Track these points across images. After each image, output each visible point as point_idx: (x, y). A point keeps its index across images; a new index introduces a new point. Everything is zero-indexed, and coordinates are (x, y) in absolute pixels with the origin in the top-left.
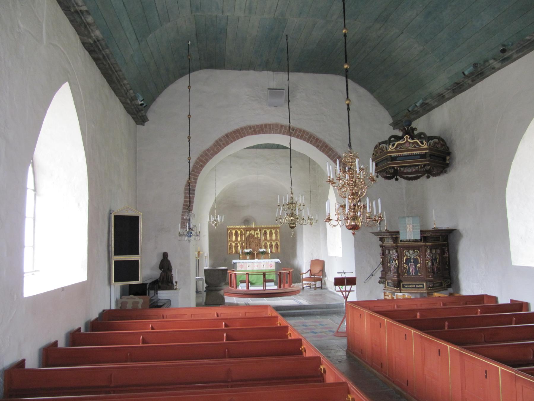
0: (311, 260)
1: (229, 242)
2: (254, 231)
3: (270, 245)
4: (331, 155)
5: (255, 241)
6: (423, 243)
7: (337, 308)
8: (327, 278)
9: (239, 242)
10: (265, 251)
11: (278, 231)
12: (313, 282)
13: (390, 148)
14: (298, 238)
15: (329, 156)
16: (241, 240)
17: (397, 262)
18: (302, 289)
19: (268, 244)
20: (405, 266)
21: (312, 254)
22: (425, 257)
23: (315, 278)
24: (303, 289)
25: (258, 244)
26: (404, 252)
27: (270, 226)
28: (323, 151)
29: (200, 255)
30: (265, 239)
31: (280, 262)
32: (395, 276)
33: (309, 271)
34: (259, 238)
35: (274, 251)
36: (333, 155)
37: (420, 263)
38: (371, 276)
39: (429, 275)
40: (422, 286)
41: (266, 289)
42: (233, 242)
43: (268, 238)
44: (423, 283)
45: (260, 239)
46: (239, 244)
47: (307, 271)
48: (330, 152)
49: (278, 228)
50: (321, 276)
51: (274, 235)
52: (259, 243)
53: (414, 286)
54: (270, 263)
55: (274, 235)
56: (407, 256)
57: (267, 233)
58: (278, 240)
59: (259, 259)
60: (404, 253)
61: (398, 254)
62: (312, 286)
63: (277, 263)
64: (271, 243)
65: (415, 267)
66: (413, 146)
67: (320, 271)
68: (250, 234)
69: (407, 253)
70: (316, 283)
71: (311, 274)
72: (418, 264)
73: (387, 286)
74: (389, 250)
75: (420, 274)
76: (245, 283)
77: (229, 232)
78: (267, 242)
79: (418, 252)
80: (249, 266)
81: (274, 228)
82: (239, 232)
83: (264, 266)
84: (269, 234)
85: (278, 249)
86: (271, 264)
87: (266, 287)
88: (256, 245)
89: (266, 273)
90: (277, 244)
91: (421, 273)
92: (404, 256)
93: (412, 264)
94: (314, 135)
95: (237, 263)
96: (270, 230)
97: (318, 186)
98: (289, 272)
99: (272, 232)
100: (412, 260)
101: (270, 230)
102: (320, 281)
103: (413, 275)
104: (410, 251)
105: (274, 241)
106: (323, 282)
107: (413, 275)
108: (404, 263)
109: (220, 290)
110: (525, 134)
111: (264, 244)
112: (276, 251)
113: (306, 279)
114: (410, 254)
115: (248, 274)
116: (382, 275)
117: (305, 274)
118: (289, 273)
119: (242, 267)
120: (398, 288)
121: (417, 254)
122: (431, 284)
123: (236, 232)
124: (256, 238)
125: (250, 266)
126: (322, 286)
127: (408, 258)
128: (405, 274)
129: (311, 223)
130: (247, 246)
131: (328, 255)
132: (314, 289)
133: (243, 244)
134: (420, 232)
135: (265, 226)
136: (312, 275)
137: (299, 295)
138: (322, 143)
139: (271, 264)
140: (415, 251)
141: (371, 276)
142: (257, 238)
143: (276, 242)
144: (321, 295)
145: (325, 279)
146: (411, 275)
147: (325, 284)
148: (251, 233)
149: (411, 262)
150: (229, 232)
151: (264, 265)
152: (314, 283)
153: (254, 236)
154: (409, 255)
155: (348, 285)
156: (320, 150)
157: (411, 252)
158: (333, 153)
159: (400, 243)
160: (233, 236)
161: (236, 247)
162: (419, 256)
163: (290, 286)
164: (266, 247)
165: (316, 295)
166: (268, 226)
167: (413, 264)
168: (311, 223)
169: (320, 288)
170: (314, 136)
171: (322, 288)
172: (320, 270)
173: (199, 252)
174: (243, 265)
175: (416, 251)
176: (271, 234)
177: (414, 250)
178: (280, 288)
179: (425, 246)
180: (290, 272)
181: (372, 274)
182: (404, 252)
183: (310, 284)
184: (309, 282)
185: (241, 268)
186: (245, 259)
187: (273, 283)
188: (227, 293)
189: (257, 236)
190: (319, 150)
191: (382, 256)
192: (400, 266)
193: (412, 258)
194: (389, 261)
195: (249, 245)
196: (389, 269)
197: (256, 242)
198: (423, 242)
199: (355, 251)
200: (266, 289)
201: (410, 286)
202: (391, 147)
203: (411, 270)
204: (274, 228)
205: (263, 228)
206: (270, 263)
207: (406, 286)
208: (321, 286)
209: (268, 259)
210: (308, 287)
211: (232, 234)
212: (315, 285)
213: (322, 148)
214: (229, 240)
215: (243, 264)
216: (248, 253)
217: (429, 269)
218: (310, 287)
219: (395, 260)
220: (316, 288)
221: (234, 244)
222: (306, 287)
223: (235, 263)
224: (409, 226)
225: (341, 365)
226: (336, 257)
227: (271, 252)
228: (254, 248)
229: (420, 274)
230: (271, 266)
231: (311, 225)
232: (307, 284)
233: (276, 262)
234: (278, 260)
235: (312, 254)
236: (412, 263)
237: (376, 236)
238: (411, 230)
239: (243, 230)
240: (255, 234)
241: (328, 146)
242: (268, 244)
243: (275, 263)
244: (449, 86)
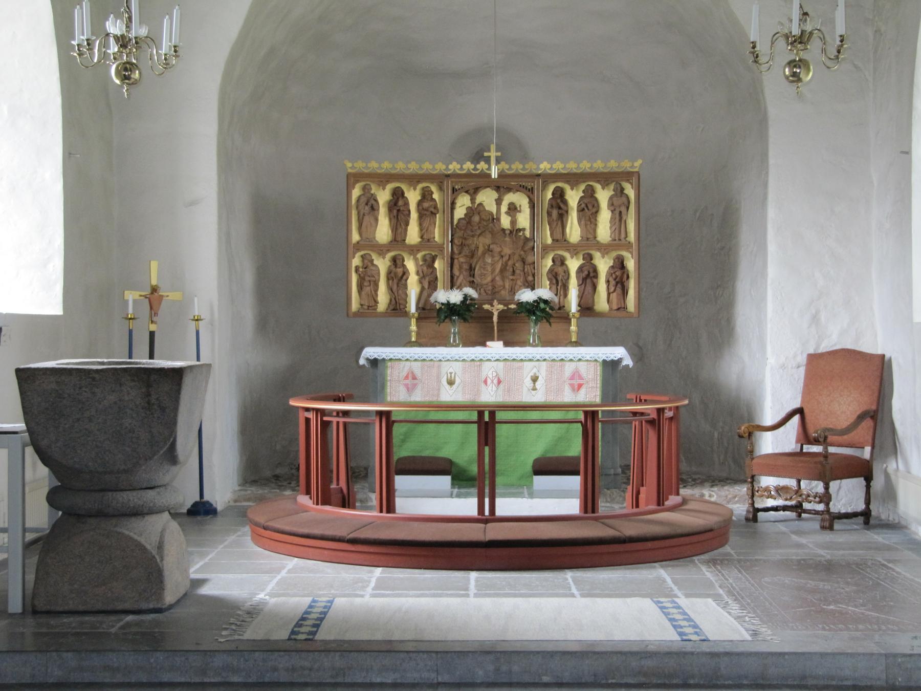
0: (812, 351)
1: (358, 250)
2: (494, 195)
3: (580, 270)
5: (496, 249)
9: (413, 250)
10: (546, 302)
11: (630, 192)
12: (815, 483)
14: (746, 236)
16: (426, 239)
18: (747, 519)
19: (574, 264)
21: (815, 319)
23: (826, 455)
24: (755, 519)
25: (519, 265)
27: (585, 166)
29: (163, 309)
30: (558, 236)
31: (628, 361)
33: (796, 419)
34: (524, 230)
35: (602, 302)
41: (499, 512)
42: (381, 250)
43: (574, 231)
45: (527, 240)
46: (410, 265)
47: (782, 415)
49: (628, 175)
50: (868, 449)
51: (605, 216)
52: (524, 261)
54: (569, 368)
55: (605, 216)
57: (565, 202)
58: (628, 247)
59: (507, 344)
62: (806, 506)
63: (611, 366)
64: (589, 258)
67: (861, 417)
68: (475, 210)
70: (831, 490)
71: (805, 437)
76: (576, 473)
77: (356, 192)
78: (567, 255)
80: (451, 383)
81: (605, 178)
82: (413, 197)
83: (539, 384)
84: (581, 210)
85: (625, 292)
86: (576, 375)
87: (499, 501)
88: (503, 270)
89: (500, 416)
90: (620, 264)
95: (384, 360)
96: (583, 187)
98: (654, 415)
99: (596, 200)
101: (583, 187)
105: (605, 249)
106: (878, 483)
109: (138, 513)
110: (632, 639)
111: (549, 263)
112: (615, 307)
113: (778, 462)
115: (388, 414)
117: (769, 433)
118: (651, 422)
119: (415, 386)
123: (398, 195)
124: (504, 230)
125: (458, 381)
126: (871, 507)
129: (792, 64)
130: (456, 272)
132: (817, 526)
133: (436, 265)
135: (559, 167)
136: (809, 442)
137: (713, 562)
139: (576, 375)
142: (515, 231)
143: (614, 254)
144: (855, 568)
145: (894, 465)
147: (890, 494)
148: (480, 204)
150: (356, 192)
151: (535, 379)
152: (819, 487)
153: (495, 219)
160: (377, 220)
161: (397, 278)
163: (660, 502)
164: (559, 280)
165: (828, 568)
166: (572, 167)
168: (792, 64)
169: (861, 519)
171: (872, 522)
173: (154, 290)
174: (418, 373)
176: (589, 208)
178: (586, 512)
180: (660, 411)
183: (798, 491)
184: (791, 483)
185: (410, 389)
186: (442, 341)
187: (446, 480)
188: (265, 528)
189: (513, 222)
195: (466, 266)
197: (507, 251)
200: (499, 512)
204: (605, 178)
205: (547, 178)
206: (573, 365)
208: (861, 507)
209: (566, 346)
210: (785, 508)
211: (374, 208)
212: (826, 498)
214: (355, 237)
215: (416, 367)
216: (450, 310)
218: (798, 509)
220: (830, 521)
221: (382, 265)
222: (776, 509)
223: (374, 363)
225: (882, 513)
227: (587, 309)
228: (494, 287)
230: (576, 382)
231: (796, 78)
232: (780, 490)
233: (604, 362)
234: (618, 352)
235: (815, 319)
239: (433, 188)
240: (504, 208)
242: (574, 264)
243: (599, 369)
244: (887, 467)
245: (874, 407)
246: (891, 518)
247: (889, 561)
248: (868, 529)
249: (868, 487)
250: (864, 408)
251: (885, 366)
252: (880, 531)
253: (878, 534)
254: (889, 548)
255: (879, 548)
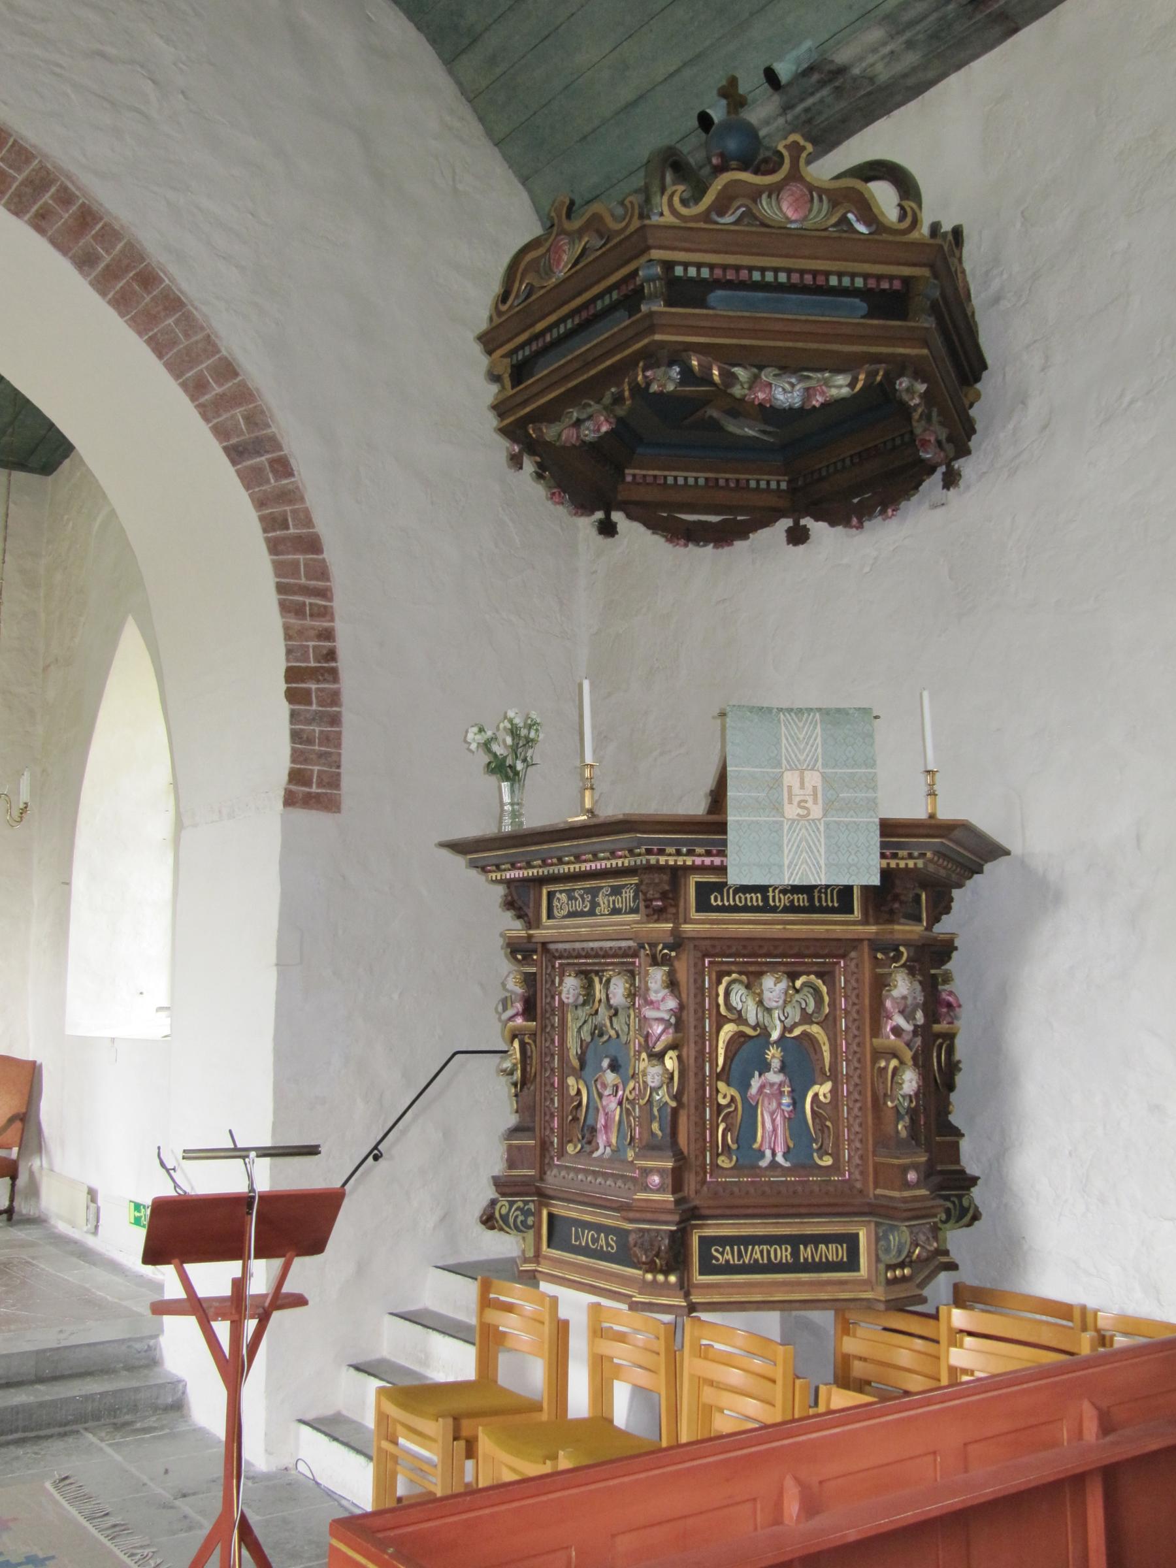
4: (174, 342)
6: (865, 921)
7: (103, 1370)
8: (50, 1163)
13: (674, 212)
15: (159, 347)
17: (670, 1062)
20: (726, 1093)
22: (876, 1031)
26: (721, 990)
28: (121, 303)
32: (656, 1179)
36: (184, 343)
37: (834, 1076)
38: (371, 1158)
39: (905, 1169)
40: (834, 1252)
44: (851, 1229)
48: (170, 321)
50: (15, 1150)
53: (783, 1254)
56: (740, 1019)
60: (721, 1000)
61: (682, 1007)
65: (797, 1103)
66: (834, 220)
67: (11, 1120)
69: (739, 996)
72: (814, 1083)
73: (556, 1253)
74: (586, 976)
75: (827, 1161)
79: (817, 992)
91: (836, 1156)
92: (720, 1022)
93: (772, 1085)
94: (69, 177)
97: (46, 668)
100: (774, 1055)
102: (7, 1180)
103: (774, 1165)
104: (768, 982)
106: (22, 1181)
107: (774, 1165)
108: (719, 1077)
114: (760, 1003)
116: (511, 1164)
120: (666, 1273)
121: (810, 1010)
122: (922, 1238)
126: (15, 1204)
127: (749, 1032)
128: (723, 1162)
131: (69, 1031)
134: (876, 839)
138: (119, 246)
140: (798, 984)
141: (371, 1158)
146: (764, 1163)
147: (34, 1191)
149: (765, 1067)
154: (752, 1013)
155: (262, 1252)
156: (103, 294)
157: (773, 987)
158: (187, 336)
159: (694, 915)
162: (829, 1023)
167: (781, 1085)
170: (64, 189)
171: (15, 1217)
172: (9, 1115)
175: (804, 985)
177: (793, 977)
179: (876, 945)
181: (376, 1148)
182: (721, 990)
190: (91, 284)
191: (519, 1021)
192: (689, 1097)
193: (775, 1035)
194: (575, 1063)
196: (575, 1119)
198: (865, 912)
199: (279, 992)
201: (756, 1253)
202: (676, 200)
203: (769, 1125)
207: (726, 1256)
213: (117, 277)
217: (899, 1116)
219: (658, 1048)
224: (802, 786)
226: (113, 1040)
229: (827, 1161)
236: (774, 1077)
237: (484, 869)
238: (816, 811)
241: (161, 281)
245: (24, 1110)
246: (32, 1213)
247: (33, 1258)
248: (11, 1226)
249: (13, 1185)
250: (14, 1111)
251: (36, 1070)
252: (21, 1227)
253: (21, 1230)
254: (32, 1245)
255: (23, 1245)
